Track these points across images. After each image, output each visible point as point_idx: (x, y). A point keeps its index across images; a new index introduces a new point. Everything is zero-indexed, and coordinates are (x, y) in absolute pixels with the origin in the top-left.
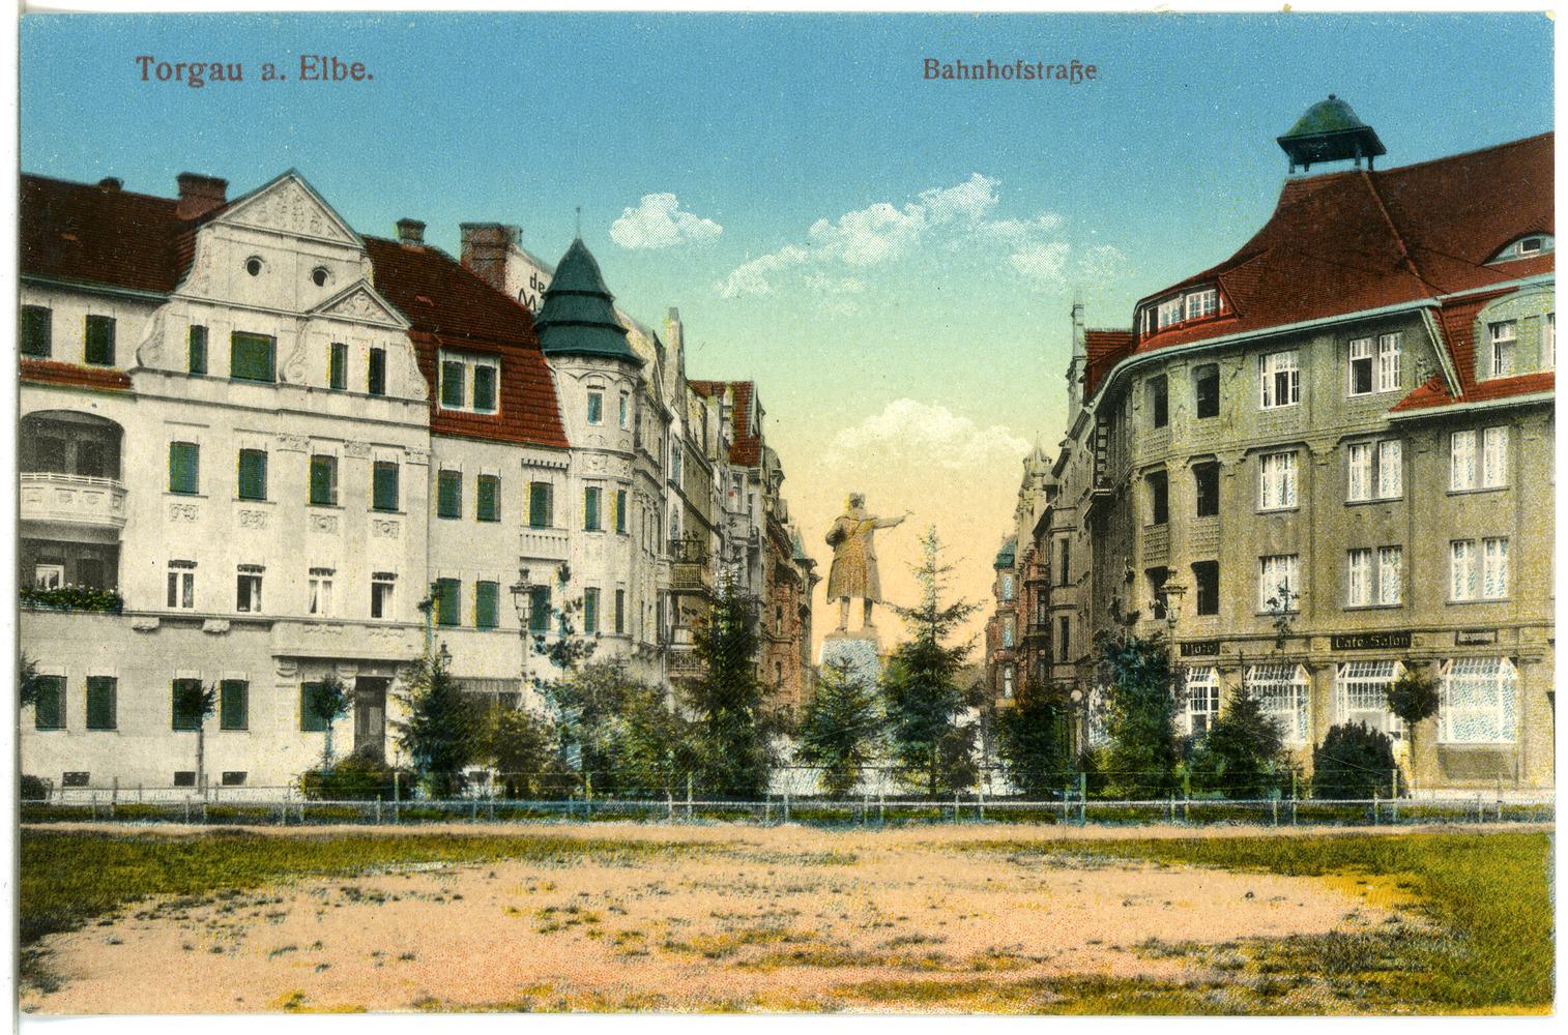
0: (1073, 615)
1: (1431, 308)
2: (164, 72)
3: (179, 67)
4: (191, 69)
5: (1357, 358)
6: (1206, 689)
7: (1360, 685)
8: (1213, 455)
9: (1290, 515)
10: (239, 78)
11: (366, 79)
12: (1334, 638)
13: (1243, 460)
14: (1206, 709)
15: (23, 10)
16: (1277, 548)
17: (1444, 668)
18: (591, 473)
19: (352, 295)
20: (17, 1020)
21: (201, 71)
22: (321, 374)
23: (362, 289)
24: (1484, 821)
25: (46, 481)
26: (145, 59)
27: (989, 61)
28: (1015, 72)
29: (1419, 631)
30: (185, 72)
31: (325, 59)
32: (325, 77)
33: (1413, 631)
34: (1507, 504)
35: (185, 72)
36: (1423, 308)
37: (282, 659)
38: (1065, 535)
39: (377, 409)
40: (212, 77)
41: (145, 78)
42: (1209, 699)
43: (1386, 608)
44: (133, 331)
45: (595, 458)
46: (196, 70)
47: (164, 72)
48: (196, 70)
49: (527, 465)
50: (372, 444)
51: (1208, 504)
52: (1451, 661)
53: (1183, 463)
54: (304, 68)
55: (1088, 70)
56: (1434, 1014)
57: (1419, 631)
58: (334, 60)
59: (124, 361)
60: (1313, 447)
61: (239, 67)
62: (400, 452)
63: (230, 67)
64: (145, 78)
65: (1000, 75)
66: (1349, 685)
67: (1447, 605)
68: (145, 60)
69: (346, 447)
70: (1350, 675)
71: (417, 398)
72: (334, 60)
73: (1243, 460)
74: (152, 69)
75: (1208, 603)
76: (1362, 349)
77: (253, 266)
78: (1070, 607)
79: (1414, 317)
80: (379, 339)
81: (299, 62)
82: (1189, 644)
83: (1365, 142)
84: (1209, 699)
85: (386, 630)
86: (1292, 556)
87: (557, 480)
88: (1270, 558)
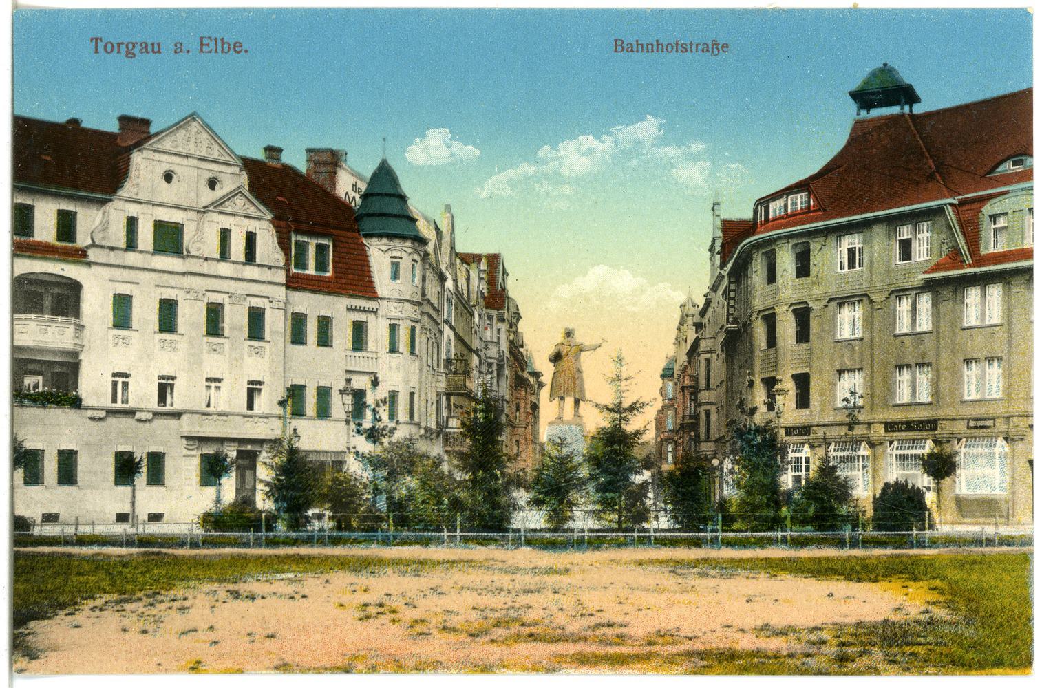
0: (713, 409)
1: (951, 205)
2: (109, 48)
3: (119, 45)
4: (127, 46)
5: (902, 238)
6: (801, 458)
7: (904, 455)
8: (806, 303)
9: (857, 343)
10: (159, 52)
11: (243, 53)
12: (886, 424)
13: (826, 306)
14: (801, 471)
15: (16, 6)
16: (849, 364)
17: (960, 444)
18: (393, 314)
19: (234, 196)
20: (11, 678)
21: (134, 47)
22: (213, 249)
23: (240, 192)
24: (986, 546)
25: (31, 320)
26: (97, 39)
27: (657, 41)
28: (675, 48)
29: (943, 420)
30: (123, 48)
31: (216, 39)
32: (216, 51)
33: (939, 420)
34: (1001, 335)
35: (123, 48)
36: (945, 204)
37: (188, 438)
38: (708, 356)
39: (251, 272)
40: (141, 51)
41: (96, 52)
42: (804, 464)
43: (921, 404)
44: (88, 220)
45: (395, 305)
46: (130, 47)
47: (109, 48)
48: (130, 47)
49: (350, 309)
50: (247, 295)
51: (803, 335)
52: (964, 440)
53: (786, 308)
54: (202, 45)
55: (723, 47)
56: (953, 674)
57: (943, 420)
58: (222, 40)
59: (82, 240)
60: (873, 297)
61: (159, 44)
62: (266, 300)
63: (153, 44)
64: (96, 52)
65: (665, 50)
66: (896, 455)
67: (962, 402)
68: (96, 40)
69: (230, 297)
70: (897, 449)
71: (277, 264)
72: (222, 40)
73: (826, 306)
74: (101, 46)
75: (803, 401)
76: (905, 232)
77: (168, 177)
78: (711, 404)
79: (940, 211)
80: (252, 226)
81: (199, 41)
82: (790, 428)
83: (907, 95)
84: (804, 464)
85: (256, 419)
86: (859, 370)
87: (370, 319)
88: (844, 371)
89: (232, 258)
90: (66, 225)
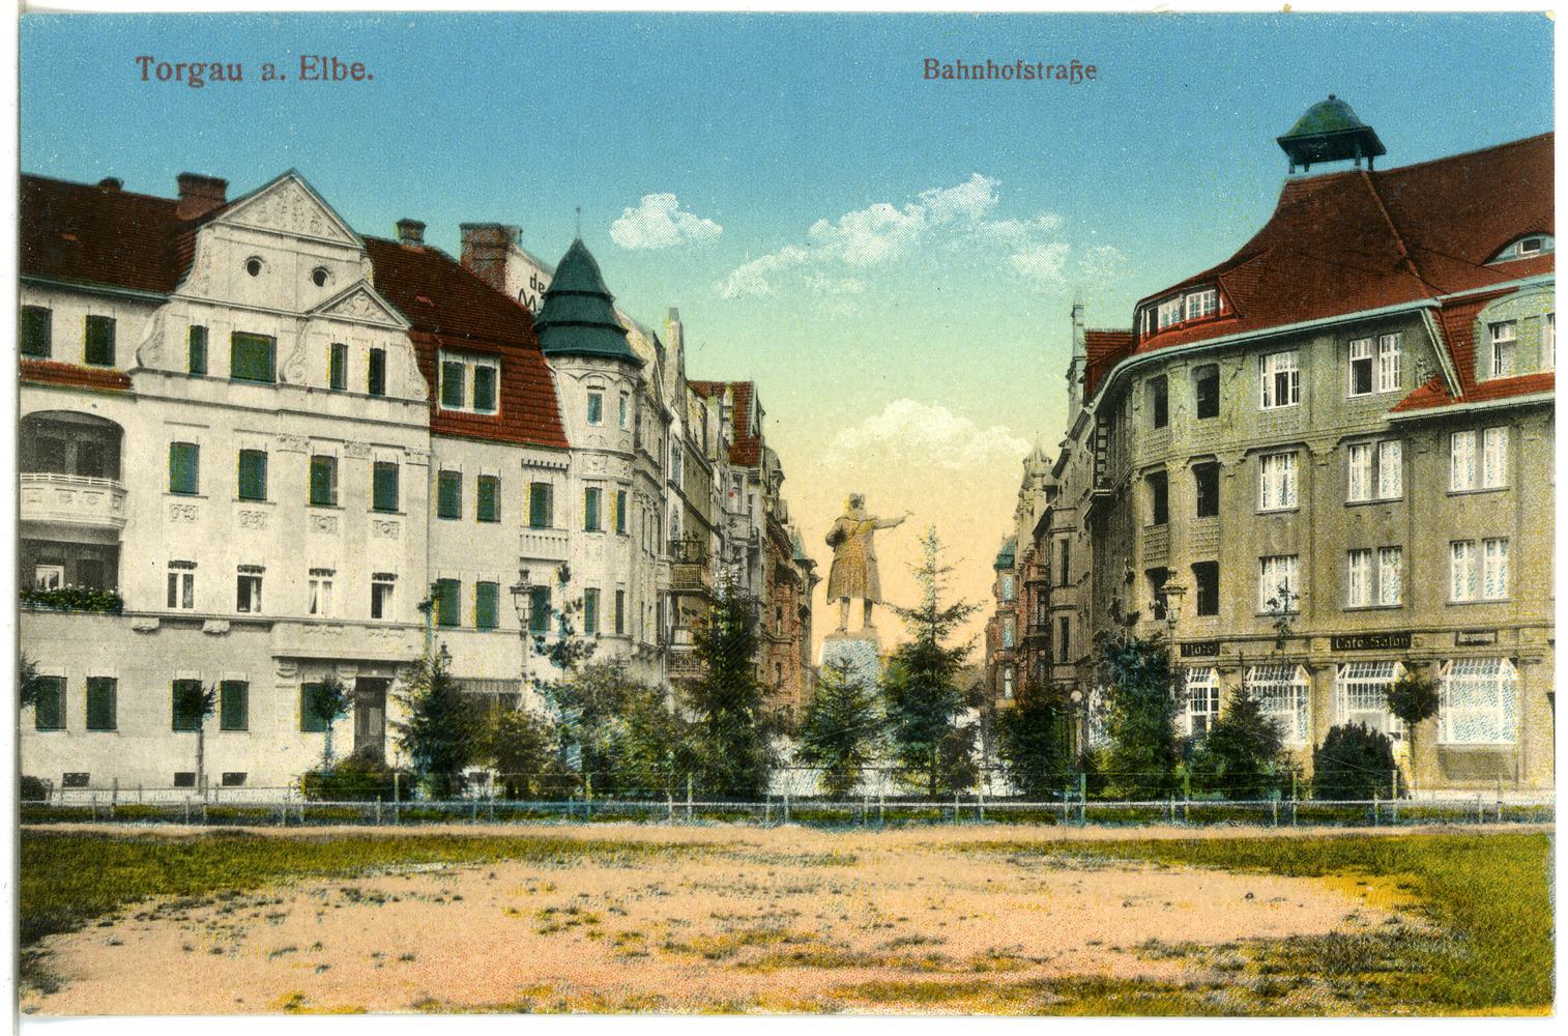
0: (1073, 616)
1: (1431, 308)
2: (164, 72)
3: (179, 67)
4: (191, 69)
5: (1357, 358)
6: (1206, 689)
7: (1360, 685)
8: (1213, 456)
9: (1290, 516)
10: (239, 78)
11: (366, 79)
12: (1334, 638)
13: (1243, 461)
14: (1206, 709)
15: (23, 10)
16: (1277, 548)
17: (1444, 669)
18: (591, 473)
19: (352, 296)
20: (17, 1021)
21: (201, 71)
22: (321, 375)
23: (362, 289)
24: (1484, 821)
25: (46, 481)
26: (145, 59)
27: (989, 62)
28: (1015, 72)
29: (1419, 632)
30: (185, 73)
31: (325, 59)
32: (325, 77)
33: (1413, 632)
34: (1507, 504)
35: (185, 73)
36: (1423, 308)
37: (282, 659)
38: (1065, 536)
39: (377, 409)
40: (212, 77)
41: (145, 78)
42: (1209, 699)
43: (1386, 608)
44: (133, 331)
45: (595, 459)
46: (196, 70)
47: (164, 72)
48: (196, 70)
49: (527, 466)
50: (372, 444)
51: (1208, 504)
52: (1451, 662)
53: (1183, 463)
54: (304, 68)
55: (1088, 71)
56: (1434, 1015)
57: (1419, 632)
58: (334, 60)
59: (124, 361)
60: (1313, 447)
61: (239, 67)
62: (400, 452)
63: (230, 67)
64: (145, 78)
65: (1000, 75)
66: (1349, 685)
67: (1447, 605)
68: (145, 60)
69: (346, 447)
70: (1350, 676)
71: (417, 398)
72: (334, 60)
73: (1243, 461)
74: (152, 69)
75: (1208, 604)
76: (1362, 350)
77: (253, 267)
78: (1070, 608)
80: (379, 340)
81: (299, 62)
82: (1189, 644)
83: (1365, 142)
84: (1209, 699)
85: (386, 631)
86: (1292, 557)
87: (557, 480)
88: (1270, 559)
89: (350, 389)
90: (100, 338)
